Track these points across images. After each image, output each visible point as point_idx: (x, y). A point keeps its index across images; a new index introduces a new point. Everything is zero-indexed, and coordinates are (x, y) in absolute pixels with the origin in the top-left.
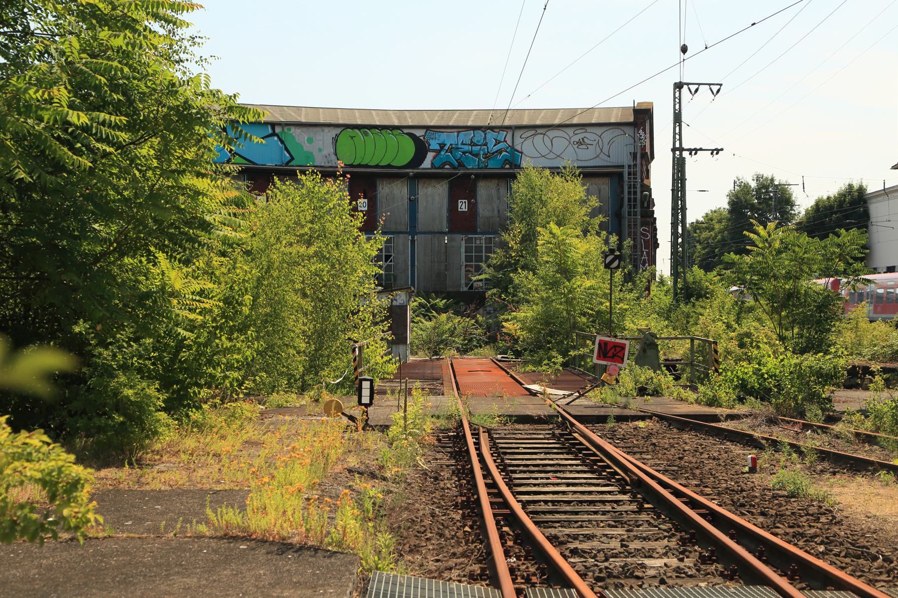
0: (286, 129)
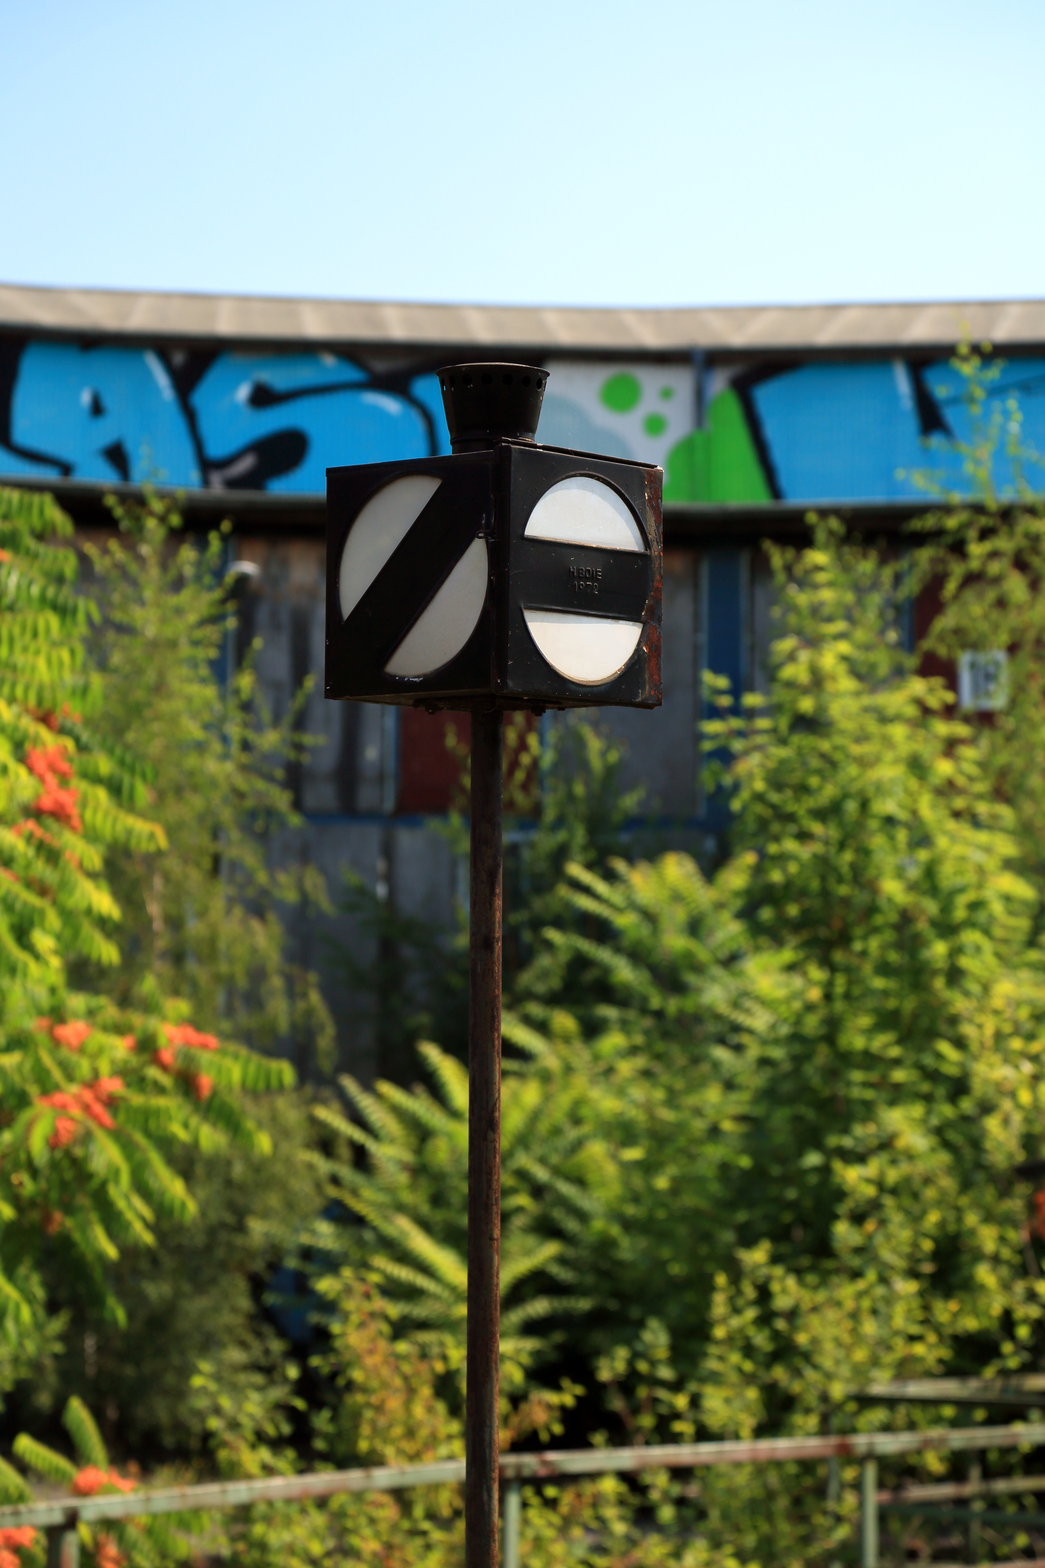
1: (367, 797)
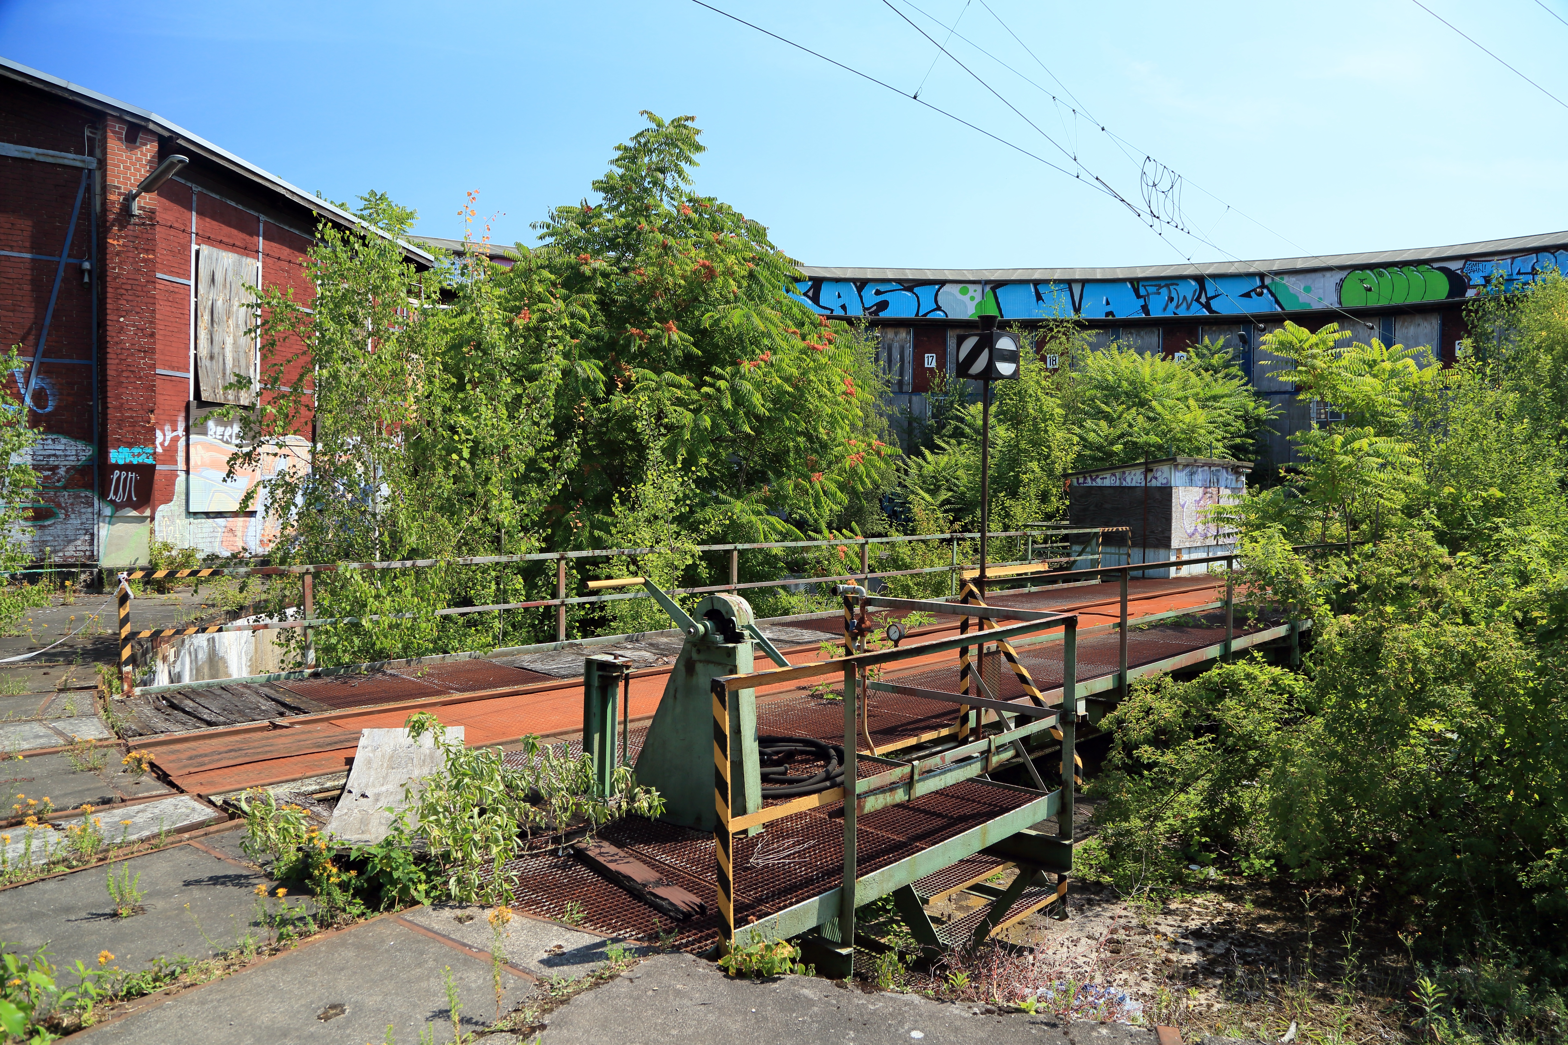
1: (905, 389)
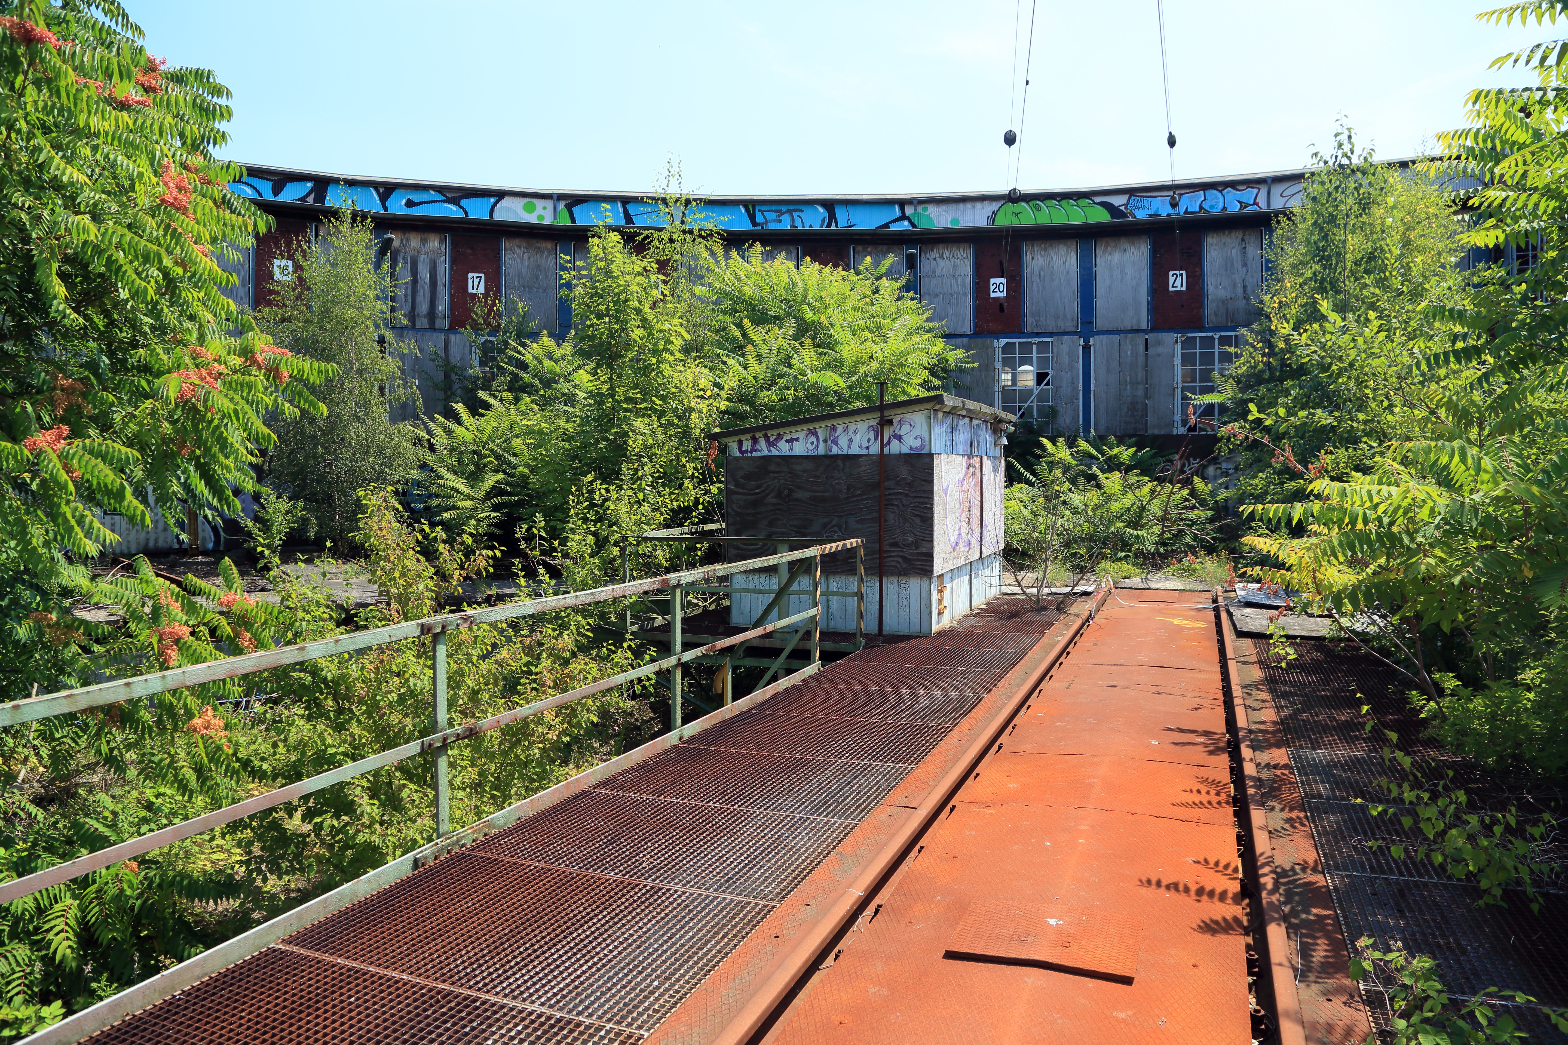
0: (920, 209)
1: (439, 323)
